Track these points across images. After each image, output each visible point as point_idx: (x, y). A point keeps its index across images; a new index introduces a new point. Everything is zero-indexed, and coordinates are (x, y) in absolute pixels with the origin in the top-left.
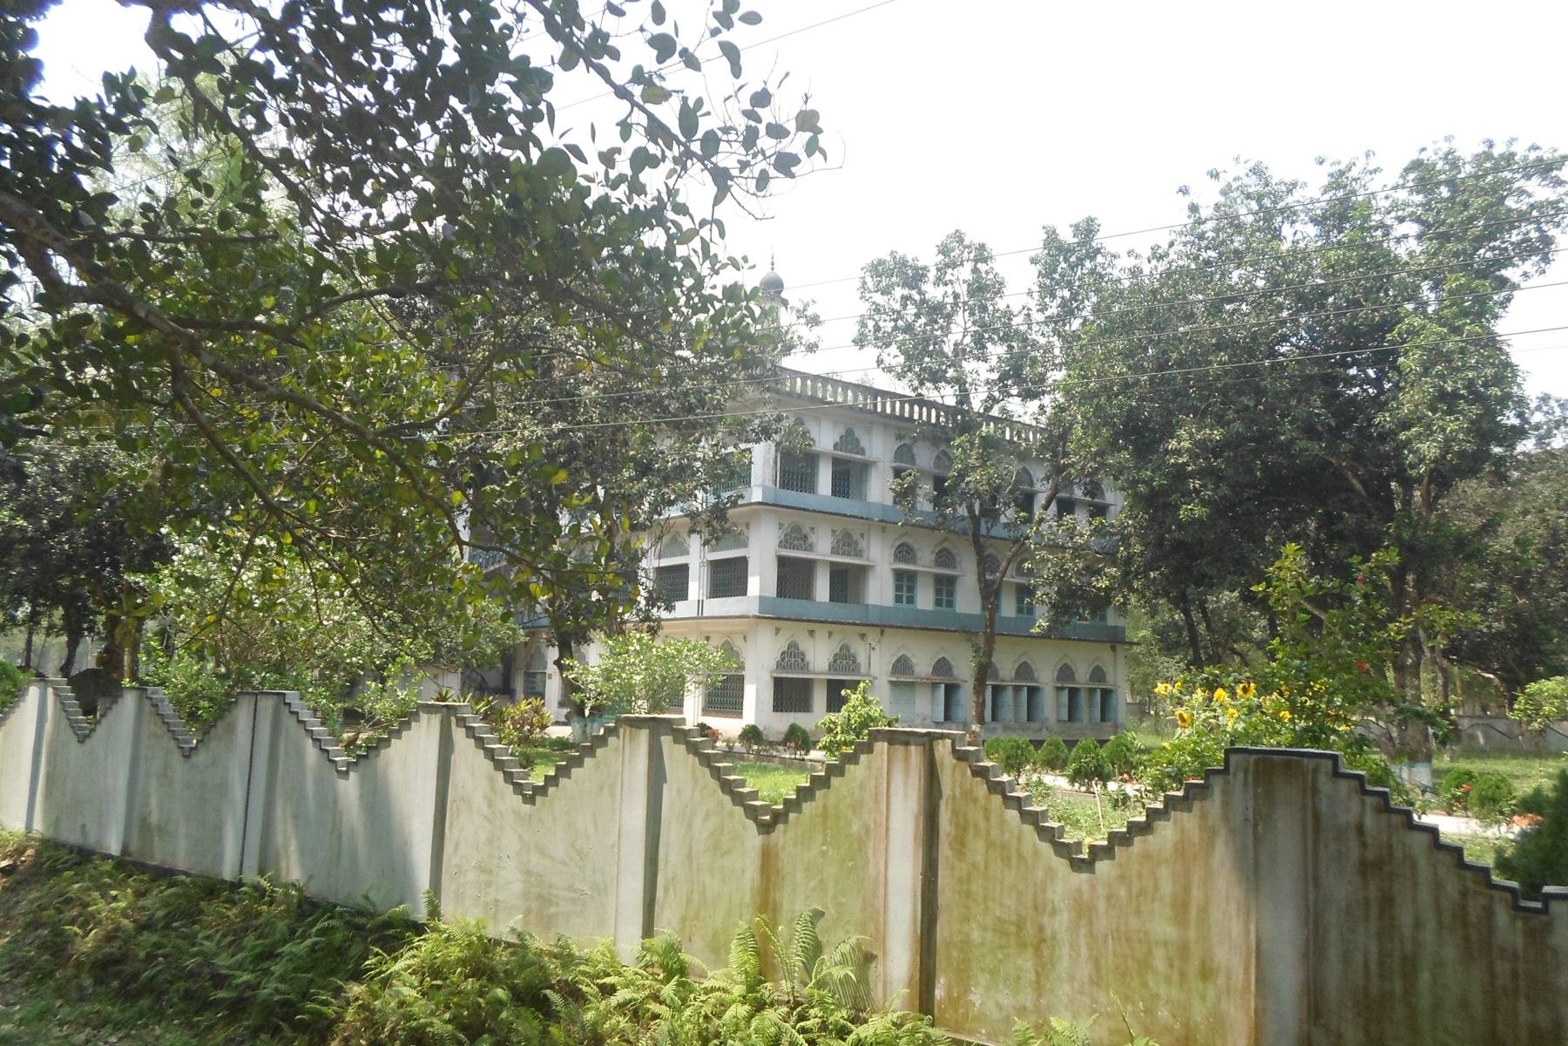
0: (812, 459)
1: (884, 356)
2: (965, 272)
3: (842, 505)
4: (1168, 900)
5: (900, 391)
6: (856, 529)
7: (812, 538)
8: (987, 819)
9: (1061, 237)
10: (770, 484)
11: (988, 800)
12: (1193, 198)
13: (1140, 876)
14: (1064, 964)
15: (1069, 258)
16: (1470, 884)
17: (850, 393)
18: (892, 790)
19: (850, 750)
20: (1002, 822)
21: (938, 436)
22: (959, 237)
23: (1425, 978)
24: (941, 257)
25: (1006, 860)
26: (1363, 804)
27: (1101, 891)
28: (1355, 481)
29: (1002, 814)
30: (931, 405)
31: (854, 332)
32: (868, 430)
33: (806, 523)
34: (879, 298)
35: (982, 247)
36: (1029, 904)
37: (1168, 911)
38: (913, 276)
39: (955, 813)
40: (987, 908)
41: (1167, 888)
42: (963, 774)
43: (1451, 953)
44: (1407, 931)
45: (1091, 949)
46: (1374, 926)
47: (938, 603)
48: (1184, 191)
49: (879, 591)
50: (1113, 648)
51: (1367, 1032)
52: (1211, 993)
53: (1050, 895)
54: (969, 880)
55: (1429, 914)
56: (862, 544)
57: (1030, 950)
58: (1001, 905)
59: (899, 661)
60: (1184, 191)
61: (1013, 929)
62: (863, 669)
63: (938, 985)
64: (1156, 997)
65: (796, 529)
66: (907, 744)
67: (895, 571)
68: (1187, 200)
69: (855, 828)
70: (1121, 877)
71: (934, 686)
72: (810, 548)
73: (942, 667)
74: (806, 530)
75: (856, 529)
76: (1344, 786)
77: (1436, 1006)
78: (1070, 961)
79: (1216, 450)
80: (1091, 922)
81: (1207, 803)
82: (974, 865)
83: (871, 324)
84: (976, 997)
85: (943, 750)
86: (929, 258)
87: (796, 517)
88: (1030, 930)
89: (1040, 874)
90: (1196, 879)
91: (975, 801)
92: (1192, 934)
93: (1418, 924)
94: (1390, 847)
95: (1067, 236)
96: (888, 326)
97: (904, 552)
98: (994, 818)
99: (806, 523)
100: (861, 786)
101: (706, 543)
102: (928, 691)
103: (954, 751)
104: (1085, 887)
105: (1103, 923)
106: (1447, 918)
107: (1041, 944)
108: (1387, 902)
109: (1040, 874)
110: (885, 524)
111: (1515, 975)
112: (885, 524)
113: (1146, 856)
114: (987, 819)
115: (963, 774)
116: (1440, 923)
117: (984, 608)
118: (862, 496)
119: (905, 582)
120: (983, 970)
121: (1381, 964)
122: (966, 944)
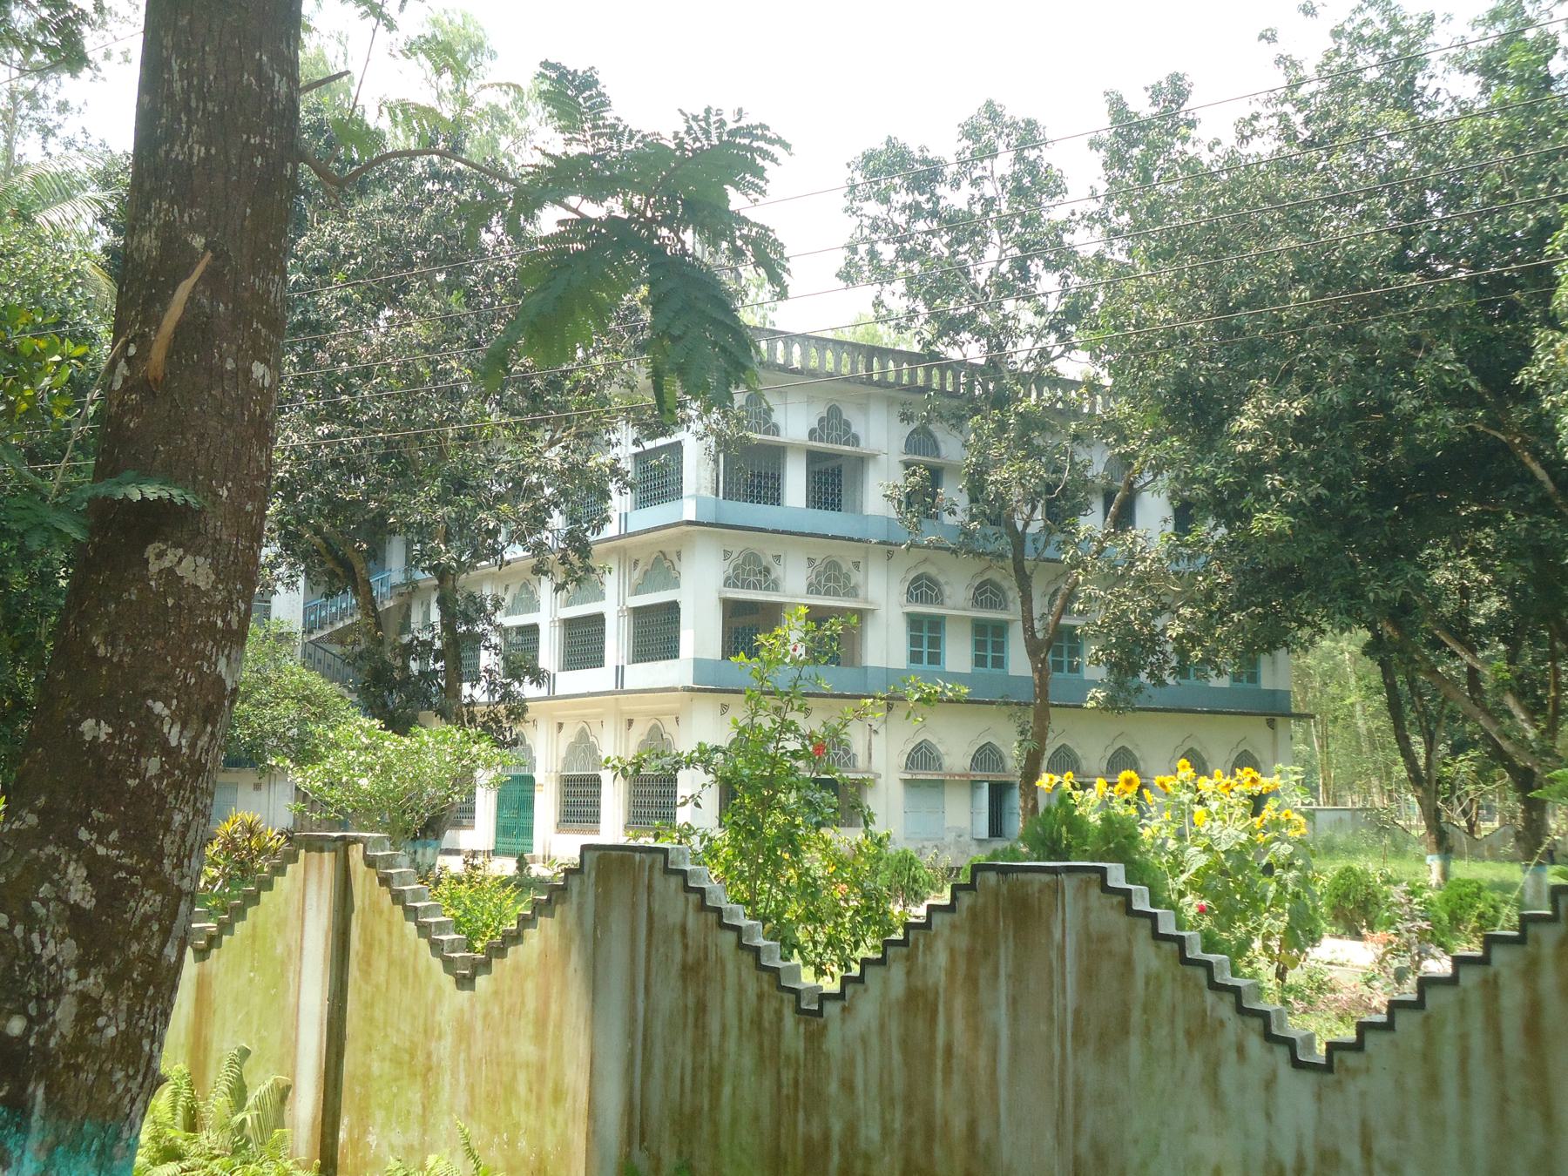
0: (777, 454)
1: (886, 297)
2: (1004, 164)
3: (827, 521)
4: (531, 1016)
5: (904, 347)
6: (846, 555)
7: (777, 571)
8: (390, 933)
9: (1131, 108)
10: (707, 493)
11: (391, 912)
12: (1284, 47)
13: (510, 991)
14: (445, 1095)
15: (1141, 139)
16: (766, 987)
17: (829, 355)
18: (308, 902)
19: (1141, 904)
20: (403, 936)
21: (959, 409)
22: (992, 112)
23: (727, 1090)
24: (966, 142)
25: (404, 980)
26: (687, 899)
27: (479, 1010)
28: (1536, 467)
29: (402, 930)
30: (947, 366)
31: (839, 260)
32: (863, 407)
33: (766, 549)
34: (873, 208)
35: (1031, 125)
36: (421, 1029)
37: (531, 1030)
38: (926, 175)
39: (364, 928)
40: (386, 1036)
41: (531, 1004)
42: (372, 882)
43: (748, 1061)
44: (715, 1040)
45: (467, 1076)
46: (690, 1034)
47: (979, 661)
48: (1268, 37)
49: (885, 646)
50: (1271, 724)
51: (680, 1154)
52: (560, 1119)
53: (438, 1017)
54: (372, 1005)
55: (732, 1021)
56: (857, 578)
57: (419, 1079)
58: (398, 1030)
59: (918, 748)
60: (1268, 37)
61: (406, 1057)
62: (861, 762)
63: (342, 1127)
64: (517, 1126)
65: (751, 558)
66: (321, 850)
67: (908, 615)
68: (1272, 51)
69: (280, 949)
70: (496, 993)
71: (975, 785)
72: (775, 586)
73: (986, 756)
74: (767, 560)
75: (846, 555)
76: (674, 882)
77: (735, 1121)
78: (452, 1091)
79: (1303, 428)
80: (469, 1047)
81: (566, 907)
82: (377, 987)
83: (863, 249)
84: (372, 1139)
85: (356, 853)
86: (946, 146)
87: (754, 542)
88: (421, 1057)
89: (430, 994)
90: (554, 991)
91: (381, 912)
92: (549, 1054)
93: (724, 1033)
94: (706, 947)
95: (1141, 106)
96: (888, 252)
97: (923, 588)
98: (395, 930)
99: (766, 549)
100: (287, 901)
101: (559, 588)
102: (966, 792)
103: (365, 856)
104: (466, 1006)
105: (478, 1049)
106: (746, 1025)
107: (427, 1073)
108: (701, 1008)
109: (430, 994)
110: (888, 547)
111: (796, 1082)
112: (888, 547)
113: (517, 968)
114: (390, 933)
115: (372, 882)
116: (740, 1028)
117: (1035, 669)
118: (856, 508)
119: (925, 634)
120: (380, 1105)
121: (694, 1077)
122: (368, 1076)
